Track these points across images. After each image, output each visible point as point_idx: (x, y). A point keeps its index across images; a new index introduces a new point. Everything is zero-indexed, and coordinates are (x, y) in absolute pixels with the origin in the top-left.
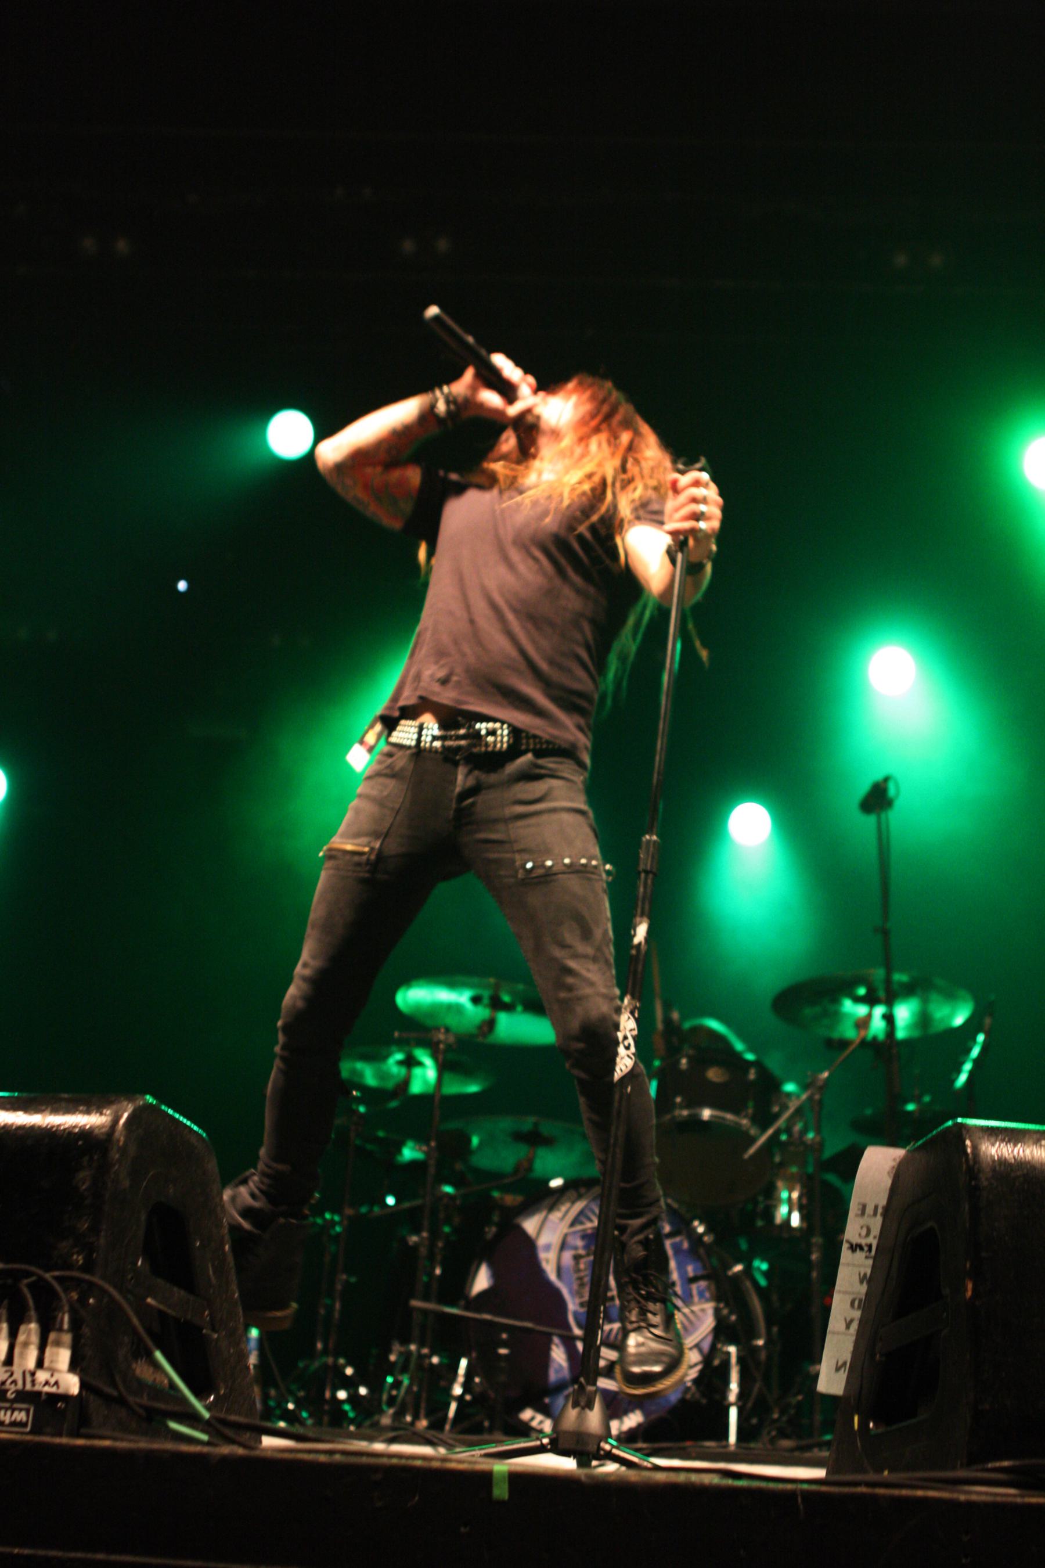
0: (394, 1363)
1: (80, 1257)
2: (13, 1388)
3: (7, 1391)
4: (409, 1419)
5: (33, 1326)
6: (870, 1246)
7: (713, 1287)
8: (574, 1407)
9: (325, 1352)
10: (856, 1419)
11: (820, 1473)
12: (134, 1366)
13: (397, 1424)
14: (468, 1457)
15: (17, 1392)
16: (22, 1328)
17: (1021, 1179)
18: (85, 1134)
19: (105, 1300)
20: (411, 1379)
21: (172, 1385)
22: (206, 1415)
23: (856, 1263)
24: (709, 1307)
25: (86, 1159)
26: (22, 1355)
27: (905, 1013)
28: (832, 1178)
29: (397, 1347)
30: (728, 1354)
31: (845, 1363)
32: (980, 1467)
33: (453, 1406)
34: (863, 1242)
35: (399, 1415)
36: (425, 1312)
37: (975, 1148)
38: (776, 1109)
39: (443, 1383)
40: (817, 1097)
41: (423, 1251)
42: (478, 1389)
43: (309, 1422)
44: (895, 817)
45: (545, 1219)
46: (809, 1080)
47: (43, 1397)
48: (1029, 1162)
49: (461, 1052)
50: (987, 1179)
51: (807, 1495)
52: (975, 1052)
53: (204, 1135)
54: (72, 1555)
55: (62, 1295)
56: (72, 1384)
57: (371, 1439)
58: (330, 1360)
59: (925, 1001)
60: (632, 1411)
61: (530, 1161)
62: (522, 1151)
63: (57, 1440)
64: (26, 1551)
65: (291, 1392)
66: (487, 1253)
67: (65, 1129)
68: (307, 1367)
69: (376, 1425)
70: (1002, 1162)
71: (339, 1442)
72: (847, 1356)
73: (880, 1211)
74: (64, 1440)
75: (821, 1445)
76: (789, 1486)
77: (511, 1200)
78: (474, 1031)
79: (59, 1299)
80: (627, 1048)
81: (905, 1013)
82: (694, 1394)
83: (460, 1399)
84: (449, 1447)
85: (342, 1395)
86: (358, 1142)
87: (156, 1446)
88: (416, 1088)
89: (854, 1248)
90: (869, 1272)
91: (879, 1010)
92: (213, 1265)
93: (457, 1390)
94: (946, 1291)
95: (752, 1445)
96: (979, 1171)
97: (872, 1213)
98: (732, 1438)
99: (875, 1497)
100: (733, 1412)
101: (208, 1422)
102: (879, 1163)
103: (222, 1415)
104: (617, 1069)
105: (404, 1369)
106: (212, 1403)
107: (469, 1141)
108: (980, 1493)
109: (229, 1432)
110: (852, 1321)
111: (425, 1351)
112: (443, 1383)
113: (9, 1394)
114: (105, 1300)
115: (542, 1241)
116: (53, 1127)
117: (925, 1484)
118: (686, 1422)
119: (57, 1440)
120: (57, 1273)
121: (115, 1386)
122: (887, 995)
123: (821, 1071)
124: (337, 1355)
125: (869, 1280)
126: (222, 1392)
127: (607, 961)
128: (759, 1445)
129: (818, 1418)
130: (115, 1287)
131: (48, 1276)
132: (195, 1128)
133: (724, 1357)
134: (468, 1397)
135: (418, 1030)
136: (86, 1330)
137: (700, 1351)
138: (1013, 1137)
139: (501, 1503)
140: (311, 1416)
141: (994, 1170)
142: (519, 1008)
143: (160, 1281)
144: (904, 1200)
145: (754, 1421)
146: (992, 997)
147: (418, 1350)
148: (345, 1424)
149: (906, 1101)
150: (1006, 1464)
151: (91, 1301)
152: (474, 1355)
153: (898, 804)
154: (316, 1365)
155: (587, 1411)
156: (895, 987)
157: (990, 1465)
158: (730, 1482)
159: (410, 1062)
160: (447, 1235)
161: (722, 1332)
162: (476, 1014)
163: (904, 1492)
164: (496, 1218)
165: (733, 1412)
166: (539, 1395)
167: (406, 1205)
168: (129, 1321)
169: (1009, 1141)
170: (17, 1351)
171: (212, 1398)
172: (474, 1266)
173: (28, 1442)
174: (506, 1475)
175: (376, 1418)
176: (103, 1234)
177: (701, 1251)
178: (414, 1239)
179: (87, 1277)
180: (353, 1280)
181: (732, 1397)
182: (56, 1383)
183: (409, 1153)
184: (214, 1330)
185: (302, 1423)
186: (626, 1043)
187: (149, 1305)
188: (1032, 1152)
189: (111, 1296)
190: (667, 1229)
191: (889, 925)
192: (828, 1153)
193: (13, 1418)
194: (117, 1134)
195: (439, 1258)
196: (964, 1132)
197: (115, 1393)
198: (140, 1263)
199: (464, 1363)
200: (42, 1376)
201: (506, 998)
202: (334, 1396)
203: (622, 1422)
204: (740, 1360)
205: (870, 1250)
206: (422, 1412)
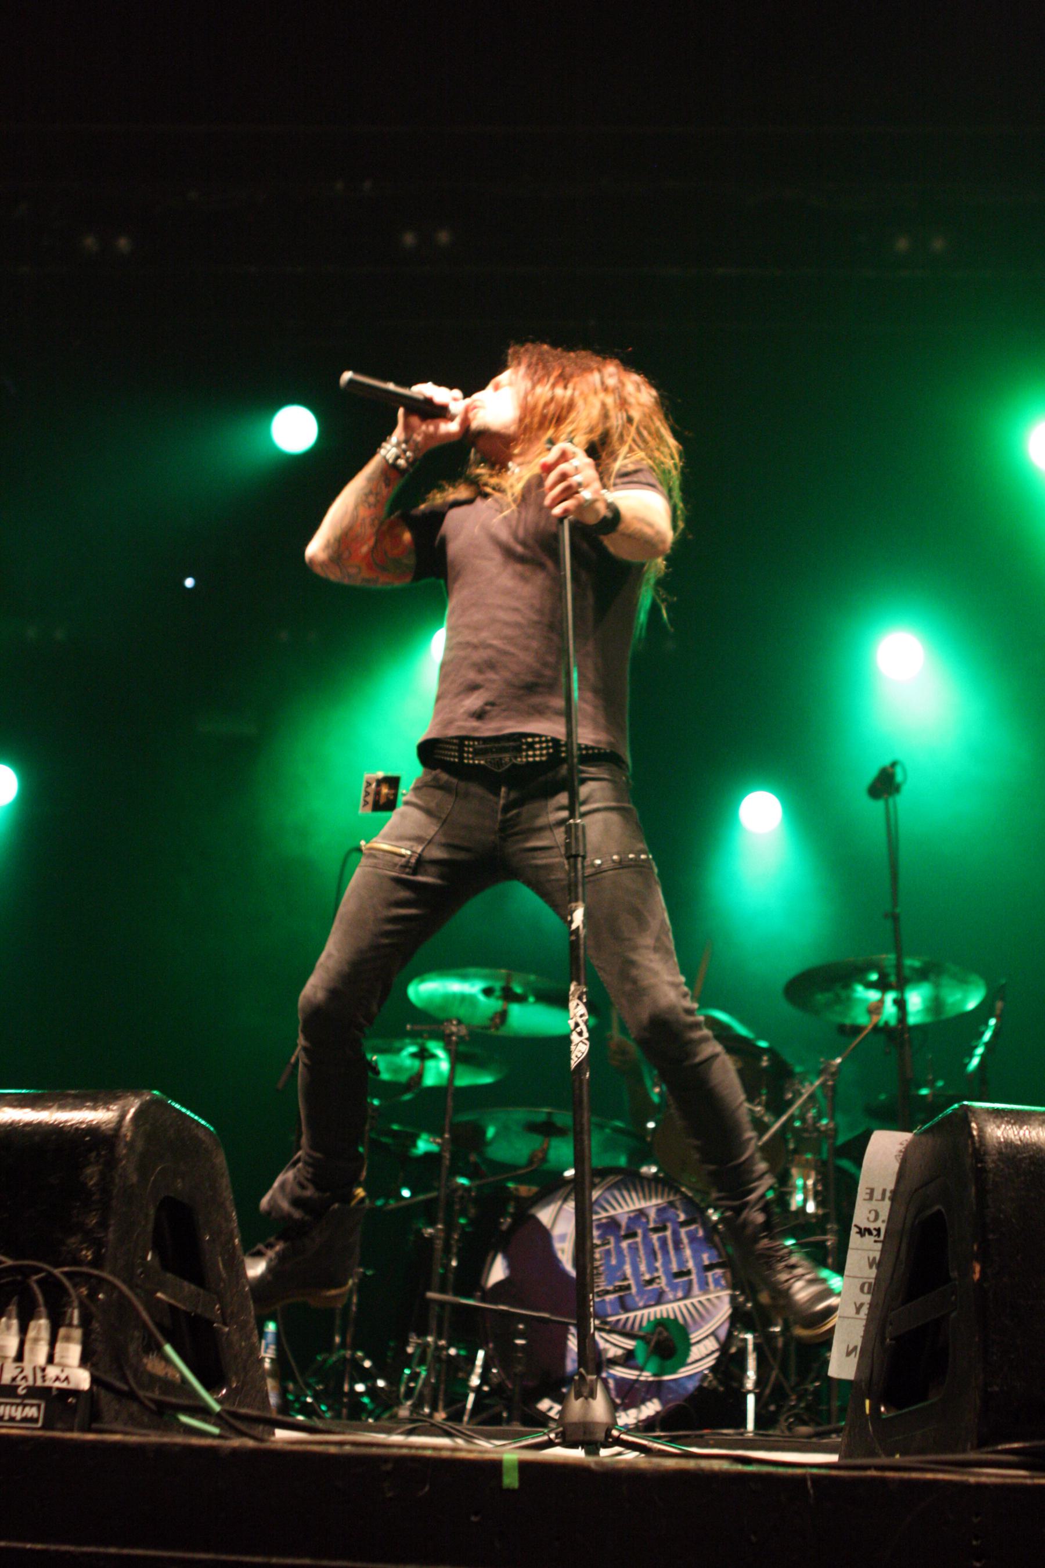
0: (411, 1355)
1: (89, 1253)
2: (24, 1384)
3: (18, 1387)
4: (427, 1410)
5: (43, 1322)
6: (878, 1230)
7: (729, 1275)
8: (577, 1397)
9: (343, 1345)
10: (867, 1402)
11: (834, 1458)
12: (145, 1360)
13: (415, 1416)
14: (486, 1447)
15: (28, 1387)
16: (32, 1324)
17: (1028, 1161)
18: (93, 1131)
19: (115, 1295)
20: (428, 1370)
21: (184, 1380)
22: (217, 1408)
23: (865, 1247)
24: (725, 1294)
25: (94, 1154)
26: (33, 1351)
27: (917, 999)
28: (846, 1164)
29: (414, 1339)
30: (745, 1340)
31: (855, 1348)
32: (990, 1449)
33: (471, 1397)
34: (872, 1226)
35: (417, 1407)
36: (442, 1304)
37: (981, 1130)
38: (789, 1096)
39: (461, 1375)
40: (830, 1083)
41: (439, 1244)
42: (495, 1380)
43: (328, 1415)
44: (902, 801)
45: (560, 1208)
46: (822, 1066)
47: (54, 1392)
48: (1035, 1144)
49: (473, 1044)
50: (993, 1162)
51: (817, 1480)
52: (987, 1036)
53: (212, 1129)
54: (85, 1549)
55: (72, 1291)
56: (83, 1379)
57: (389, 1431)
58: (348, 1353)
59: (937, 986)
60: (650, 1400)
61: (545, 1151)
62: (536, 1141)
63: (69, 1435)
64: (39, 1546)
65: (309, 1386)
66: (503, 1244)
67: (72, 1125)
68: (325, 1361)
69: (394, 1417)
70: (1009, 1144)
71: (350, 1434)
72: (858, 1341)
73: (888, 1194)
74: (75, 1435)
75: (838, 1431)
76: (790, 1471)
77: (525, 1190)
78: (487, 1023)
79: (69, 1295)
80: (580, 1034)
81: (917, 999)
82: (711, 1381)
83: (478, 1390)
84: (468, 1438)
85: (360, 1388)
86: (373, 1135)
87: (166, 1439)
88: (430, 1080)
89: (863, 1232)
90: (878, 1255)
91: (891, 996)
92: (223, 1260)
93: (475, 1381)
94: (954, 1274)
95: (771, 1432)
96: (985, 1154)
97: (880, 1197)
98: (750, 1425)
99: (883, 1481)
100: (751, 1399)
101: (219, 1415)
102: (886, 1149)
103: (233, 1409)
104: (573, 1056)
105: (422, 1361)
106: (224, 1396)
107: (484, 1133)
108: (990, 1475)
109: (238, 1424)
110: (862, 1305)
111: (442, 1343)
112: (461, 1375)
113: (20, 1389)
114: (115, 1295)
115: (556, 1232)
116: (60, 1123)
117: (932, 1466)
118: (706, 1410)
119: (69, 1435)
120: (66, 1269)
121: (127, 1382)
122: (895, 981)
123: (834, 1058)
124: (355, 1348)
125: (878, 1264)
126: (234, 1385)
127: (667, 951)
128: (777, 1432)
129: (836, 1404)
130: (124, 1281)
131: (57, 1272)
132: (203, 1122)
133: (740, 1344)
134: (486, 1388)
135: (428, 1024)
136: (96, 1325)
137: (717, 1339)
138: (1020, 1119)
139: (511, 1491)
140: (330, 1408)
141: (1000, 1153)
142: (531, 999)
143: (169, 1275)
144: (911, 1188)
145: (772, 1408)
146: (1003, 981)
147: (435, 1343)
148: (364, 1417)
149: (920, 1086)
150: (1016, 1445)
151: (101, 1296)
152: (491, 1345)
153: (905, 789)
154: (334, 1358)
155: (590, 1400)
156: (907, 972)
157: (1000, 1447)
158: (740, 1467)
159: (423, 1055)
160: (463, 1226)
161: (739, 1319)
162: (491, 1005)
163: (914, 1475)
164: (511, 1209)
165: (751, 1399)
166: (555, 1385)
167: (421, 1197)
168: (138, 1315)
169: (1014, 1124)
170: (27, 1347)
171: (224, 1391)
172: (489, 1258)
173: (40, 1437)
174: (516, 1463)
175: (395, 1409)
176: (111, 1229)
177: (717, 1239)
178: (430, 1230)
179: (96, 1272)
180: (369, 1273)
181: (750, 1384)
182: (67, 1378)
183: (424, 1145)
184: (225, 1324)
185: (320, 1417)
186: (578, 1030)
187: (159, 1300)
188: (1038, 1133)
189: (121, 1292)
190: (682, 1217)
191: (898, 910)
192: (841, 1140)
193: (24, 1414)
194: (124, 1130)
195: (455, 1250)
196: (970, 1114)
197: (125, 1388)
198: (149, 1258)
199: (481, 1354)
200: (52, 1372)
201: (518, 990)
202: (352, 1389)
203: (640, 1411)
204: (757, 1347)
205: (879, 1235)
206: (441, 1404)
